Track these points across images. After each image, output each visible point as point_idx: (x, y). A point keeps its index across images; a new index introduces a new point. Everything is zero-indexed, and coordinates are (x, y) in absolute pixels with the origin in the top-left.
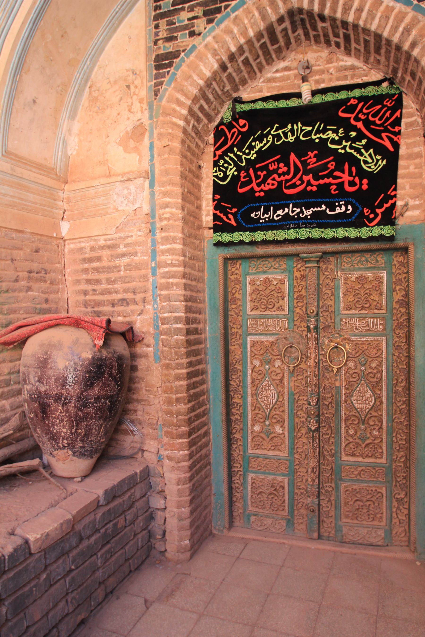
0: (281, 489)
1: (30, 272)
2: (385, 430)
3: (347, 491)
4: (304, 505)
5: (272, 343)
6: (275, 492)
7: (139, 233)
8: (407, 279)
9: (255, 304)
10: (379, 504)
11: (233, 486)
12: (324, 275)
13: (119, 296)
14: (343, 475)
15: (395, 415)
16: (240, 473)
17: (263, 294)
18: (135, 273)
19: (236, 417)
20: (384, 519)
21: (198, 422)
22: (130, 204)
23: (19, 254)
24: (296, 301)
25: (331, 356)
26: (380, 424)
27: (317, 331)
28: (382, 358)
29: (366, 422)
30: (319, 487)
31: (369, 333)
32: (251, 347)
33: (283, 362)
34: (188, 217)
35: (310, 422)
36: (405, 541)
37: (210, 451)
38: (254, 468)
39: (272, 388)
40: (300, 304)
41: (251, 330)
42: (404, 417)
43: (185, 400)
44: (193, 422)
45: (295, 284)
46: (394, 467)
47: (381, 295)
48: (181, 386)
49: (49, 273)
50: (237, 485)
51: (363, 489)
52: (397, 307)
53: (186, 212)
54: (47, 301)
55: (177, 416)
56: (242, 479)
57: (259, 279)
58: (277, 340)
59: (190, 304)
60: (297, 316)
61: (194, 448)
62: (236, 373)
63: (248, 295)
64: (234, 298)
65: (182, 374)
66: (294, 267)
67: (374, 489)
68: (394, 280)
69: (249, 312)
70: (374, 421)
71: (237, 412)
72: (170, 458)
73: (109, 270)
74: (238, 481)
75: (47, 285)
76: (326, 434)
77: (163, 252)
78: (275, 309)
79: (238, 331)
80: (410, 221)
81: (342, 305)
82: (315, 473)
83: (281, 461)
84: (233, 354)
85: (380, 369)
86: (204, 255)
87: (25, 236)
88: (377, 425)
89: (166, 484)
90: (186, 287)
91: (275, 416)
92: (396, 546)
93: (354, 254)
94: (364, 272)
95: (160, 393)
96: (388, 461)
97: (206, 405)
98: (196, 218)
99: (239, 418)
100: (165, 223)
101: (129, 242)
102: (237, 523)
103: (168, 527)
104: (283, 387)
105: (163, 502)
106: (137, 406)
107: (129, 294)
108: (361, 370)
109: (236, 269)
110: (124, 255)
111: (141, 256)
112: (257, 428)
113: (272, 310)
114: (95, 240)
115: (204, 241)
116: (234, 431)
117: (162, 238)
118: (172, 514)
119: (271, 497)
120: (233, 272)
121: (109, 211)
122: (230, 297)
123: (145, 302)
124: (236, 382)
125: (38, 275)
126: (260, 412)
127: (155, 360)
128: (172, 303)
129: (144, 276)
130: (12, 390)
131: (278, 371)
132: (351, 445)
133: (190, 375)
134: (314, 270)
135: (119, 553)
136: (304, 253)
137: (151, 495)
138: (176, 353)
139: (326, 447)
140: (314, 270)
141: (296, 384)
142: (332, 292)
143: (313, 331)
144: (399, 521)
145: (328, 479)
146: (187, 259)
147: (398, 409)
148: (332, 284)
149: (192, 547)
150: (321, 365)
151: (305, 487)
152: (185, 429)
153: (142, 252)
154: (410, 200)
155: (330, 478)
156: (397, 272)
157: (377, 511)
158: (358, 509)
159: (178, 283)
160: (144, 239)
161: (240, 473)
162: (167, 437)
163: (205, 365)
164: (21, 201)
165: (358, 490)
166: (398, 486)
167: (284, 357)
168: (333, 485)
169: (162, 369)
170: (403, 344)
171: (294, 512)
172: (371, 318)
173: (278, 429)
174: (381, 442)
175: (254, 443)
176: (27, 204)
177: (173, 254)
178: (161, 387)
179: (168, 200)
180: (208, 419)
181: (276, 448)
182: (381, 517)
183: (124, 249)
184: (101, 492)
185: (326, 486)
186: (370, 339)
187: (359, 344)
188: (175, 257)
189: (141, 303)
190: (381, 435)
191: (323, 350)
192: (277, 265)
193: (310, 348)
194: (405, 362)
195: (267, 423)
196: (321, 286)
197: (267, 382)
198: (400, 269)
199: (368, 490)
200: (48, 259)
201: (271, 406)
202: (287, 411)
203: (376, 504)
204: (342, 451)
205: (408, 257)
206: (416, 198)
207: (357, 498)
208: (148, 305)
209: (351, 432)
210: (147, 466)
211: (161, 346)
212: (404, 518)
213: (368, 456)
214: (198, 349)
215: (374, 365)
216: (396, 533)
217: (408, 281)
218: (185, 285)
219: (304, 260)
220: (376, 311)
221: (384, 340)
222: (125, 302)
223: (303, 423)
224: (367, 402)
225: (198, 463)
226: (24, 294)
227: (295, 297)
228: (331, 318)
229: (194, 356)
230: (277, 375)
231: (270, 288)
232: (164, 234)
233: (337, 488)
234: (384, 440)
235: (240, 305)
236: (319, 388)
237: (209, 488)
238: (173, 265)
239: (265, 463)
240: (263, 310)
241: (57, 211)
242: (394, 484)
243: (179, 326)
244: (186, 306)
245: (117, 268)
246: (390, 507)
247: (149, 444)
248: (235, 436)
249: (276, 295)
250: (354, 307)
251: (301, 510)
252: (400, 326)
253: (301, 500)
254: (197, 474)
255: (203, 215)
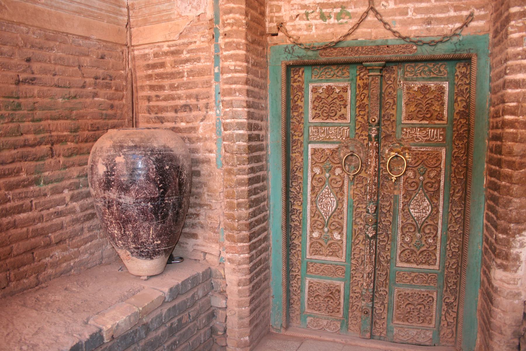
0: (337, 293)
1: (96, 78)
2: (439, 238)
3: (400, 295)
4: (359, 307)
5: (333, 152)
6: (331, 295)
7: (203, 39)
8: (468, 90)
9: (317, 111)
10: (429, 307)
11: (291, 289)
12: (387, 84)
13: (182, 102)
14: (397, 280)
15: (450, 223)
16: (298, 277)
17: (326, 102)
18: (197, 79)
19: (296, 223)
20: (433, 323)
21: (259, 227)
22: (194, 10)
23: (86, 61)
24: (358, 110)
25: (391, 165)
26: (435, 233)
27: (378, 140)
28: (441, 168)
29: (421, 230)
30: (373, 292)
31: (428, 142)
32: (312, 155)
33: (343, 170)
34: (252, 23)
35: (367, 230)
36: (451, 342)
37: (269, 255)
38: (312, 273)
39: (332, 196)
40: (362, 113)
41: (312, 138)
42: (458, 226)
43: (246, 205)
44: (254, 227)
45: (358, 92)
46: (446, 273)
47: (443, 106)
48: (242, 191)
49: (114, 79)
50: (295, 288)
51: (415, 293)
52: (458, 118)
53: (249, 17)
54: (112, 107)
55: (239, 221)
56: (299, 282)
57: (321, 87)
58: (338, 148)
59: (252, 110)
60: (358, 125)
61: (254, 252)
62: (296, 180)
63: (310, 103)
64: (296, 105)
65: (243, 180)
66: (357, 76)
67: (425, 294)
68: (456, 91)
69: (311, 120)
70: (430, 229)
71: (296, 219)
72: (230, 260)
73: (172, 75)
74: (297, 285)
75: (112, 91)
76: (383, 241)
77: (226, 58)
78: (337, 117)
79: (299, 138)
80: (474, 31)
81: (404, 115)
82: (371, 278)
83: (337, 267)
84: (294, 161)
85: (438, 179)
86: (267, 61)
87: (92, 42)
88: (433, 233)
89: (227, 285)
90: (249, 105)
91: (333, 223)
92: (443, 346)
93: (417, 63)
94: (426, 83)
95: (222, 198)
96: (441, 268)
97: (266, 211)
98: (259, 24)
99: (299, 224)
100: (228, 28)
101: (192, 48)
102: (294, 324)
103: (229, 324)
104: (342, 195)
105: (224, 301)
106: (199, 210)
107: (192, 100)
108: (420, 180)
109: (299, 77)
110: (187, 61)
111: (204, 62)
112: (316, 235)
113: (334, 118)
114: (158, 46)
115: (267, 48)
116: (293, 237)
117: (226, 44)
118: (233, 312)
119: (326, 300)
120: (295, 79)
121: (173, 17)
122: (292, 105)
123: (207, 108)
124: (296, 189)
125: (104, 81)
126: (319, 219)
127: (217, 165)
128: (234, 109)
129: (207, 82)
130: (81, 192)
131: (339, 179)
132: (406, 252)
133: (251, 181)
134: (377, 79)
135: (183, 346)
136: (367, 61)
137: (212, 296)
138: (238, 158)
139: (382, 253)
140: (377, 79)
141: (356, 192)
142: (394, 101)
143: (373, 140)
144: (448, 323)
145: (383, 284)
146: (250, 66)
147: (453, 219)
148: (394, 94)
149: (251, 342)
150: (381, 174)
151: (360, 291)
152: (246, 233)
153: (206, 58)
154: (475, 10)
155: (384, 283)
156: (459, 83)
157: (427, 314)
158: (409, 312)
159: (240, 89)
160: (207, 45)
161: (298, 277)
162: (228, 241)
163: (266, 172)
164: (87, 8)
165: (410, 295)
166: (448, 291)
167: (345, 165)
168: (387, 290)
169: (224, 174)
170: (462, 155)
171: (348, 314)
172: (431, 128)
173: (337, 236)
174: (435, 249)
175: (312, 249)
176: (93, 10)
177: (236, 60)
178: (223, 192)
179: (232, 5)
180: (268, 224)
181: (334, 254)
182: (430, 319)
183: (188, 55)
184: (166, 290)
185: (381, 291)
186: (430, 149)
187: (418, 154)
188: (238, 63)
189: (204, 109)
190: (436, 243)
191: (383, 159)
192: (340, 73)
193: (371, 157)
194: (462, 173)
195: (326, 229)
196: (383, 95)
197: (326, 190)
198: (462, 80)
199: (420, 295)
200: (113, 65)
201: (330, 213)
202: (345, 219)
203: (427, 308)
204: (398, 258)
205: (471, 68)
206: (481, 8)
207: (409, 302)
208: (210, 111)
209: (407, 239)
210: (209, 268)
211: (224, 151)
212: (452, 321)
213: (421, 263)
214: (259, 156)
215: (432, 175)
216: (444, 334)
217: (469, 92)
218: (248, 91)
219: (368, 68)
220: (437, 122)
221: (444, 151)
222: (188, 108)
223: (361, 231)
224: (424, 211)
225: (258, 266)
226: (91, 99)
227: (357, 105)
228: (393, 127)
229: (255, 162)
230: (337, 183)
231: (332, 96)
232: (227, 40)
233: (391, 293)
234: (438, 248)
235: (301, 113)
236: (378, 197)
237: (267, 290)
238: (236, 71)
239: (322, 267)
240: (325, 118)
241: (121, 18)
242: (445, 289)
243: (241, 132)
244: (248, 112)
245: (180, 74)
246: (440, 310)
247: (211, 247)
248: (294, 242)
249: (338, 103)
250: (415, 117)
251: (355, 313)
252: (460, 137)
253: (356, 303)
254: (257, 277)
255: (266, 21)
